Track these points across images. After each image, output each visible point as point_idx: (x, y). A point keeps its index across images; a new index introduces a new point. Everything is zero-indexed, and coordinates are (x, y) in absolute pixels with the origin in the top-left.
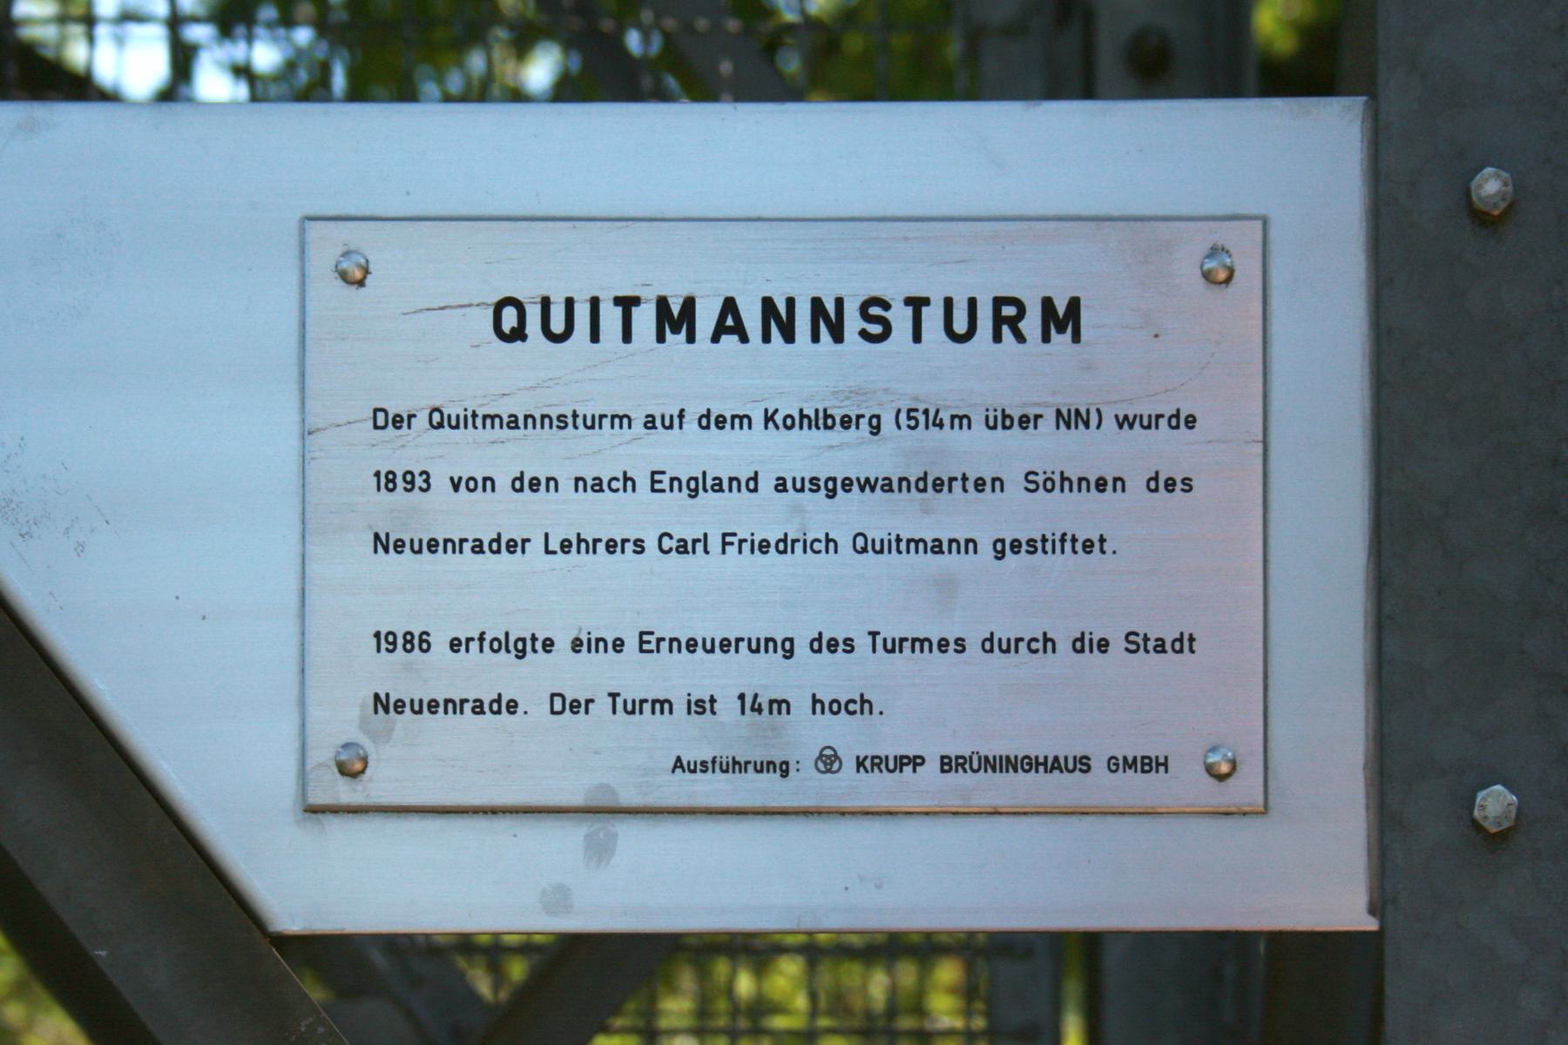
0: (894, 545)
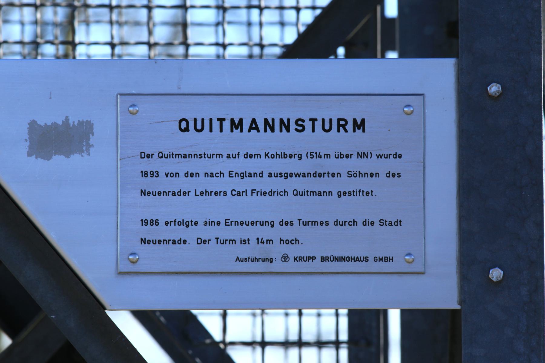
0: (171, 155)
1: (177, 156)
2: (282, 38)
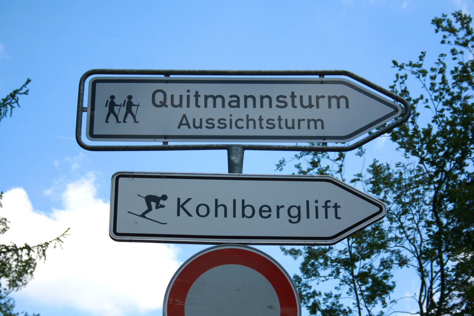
0: (193, 100)
1: (210, 100)
2: (396, 225)
